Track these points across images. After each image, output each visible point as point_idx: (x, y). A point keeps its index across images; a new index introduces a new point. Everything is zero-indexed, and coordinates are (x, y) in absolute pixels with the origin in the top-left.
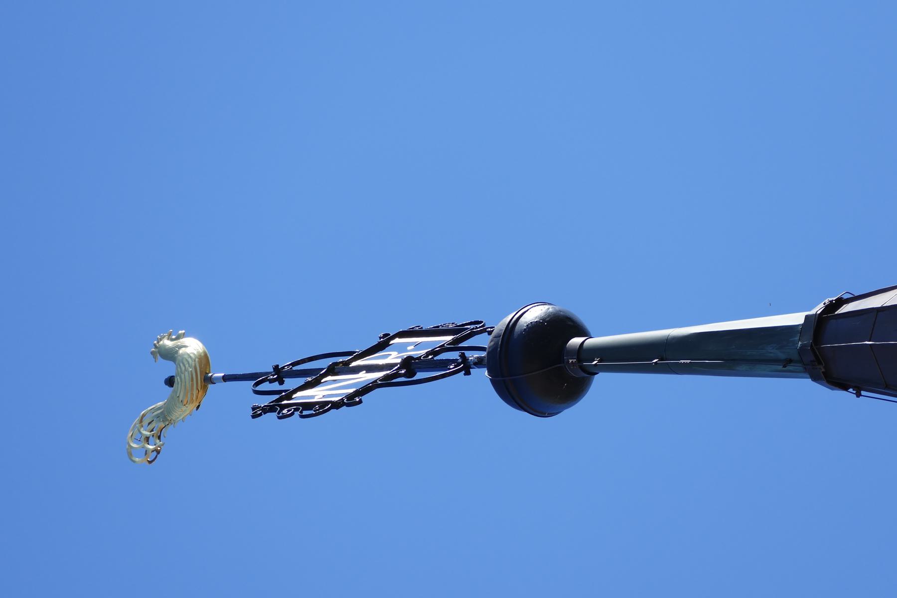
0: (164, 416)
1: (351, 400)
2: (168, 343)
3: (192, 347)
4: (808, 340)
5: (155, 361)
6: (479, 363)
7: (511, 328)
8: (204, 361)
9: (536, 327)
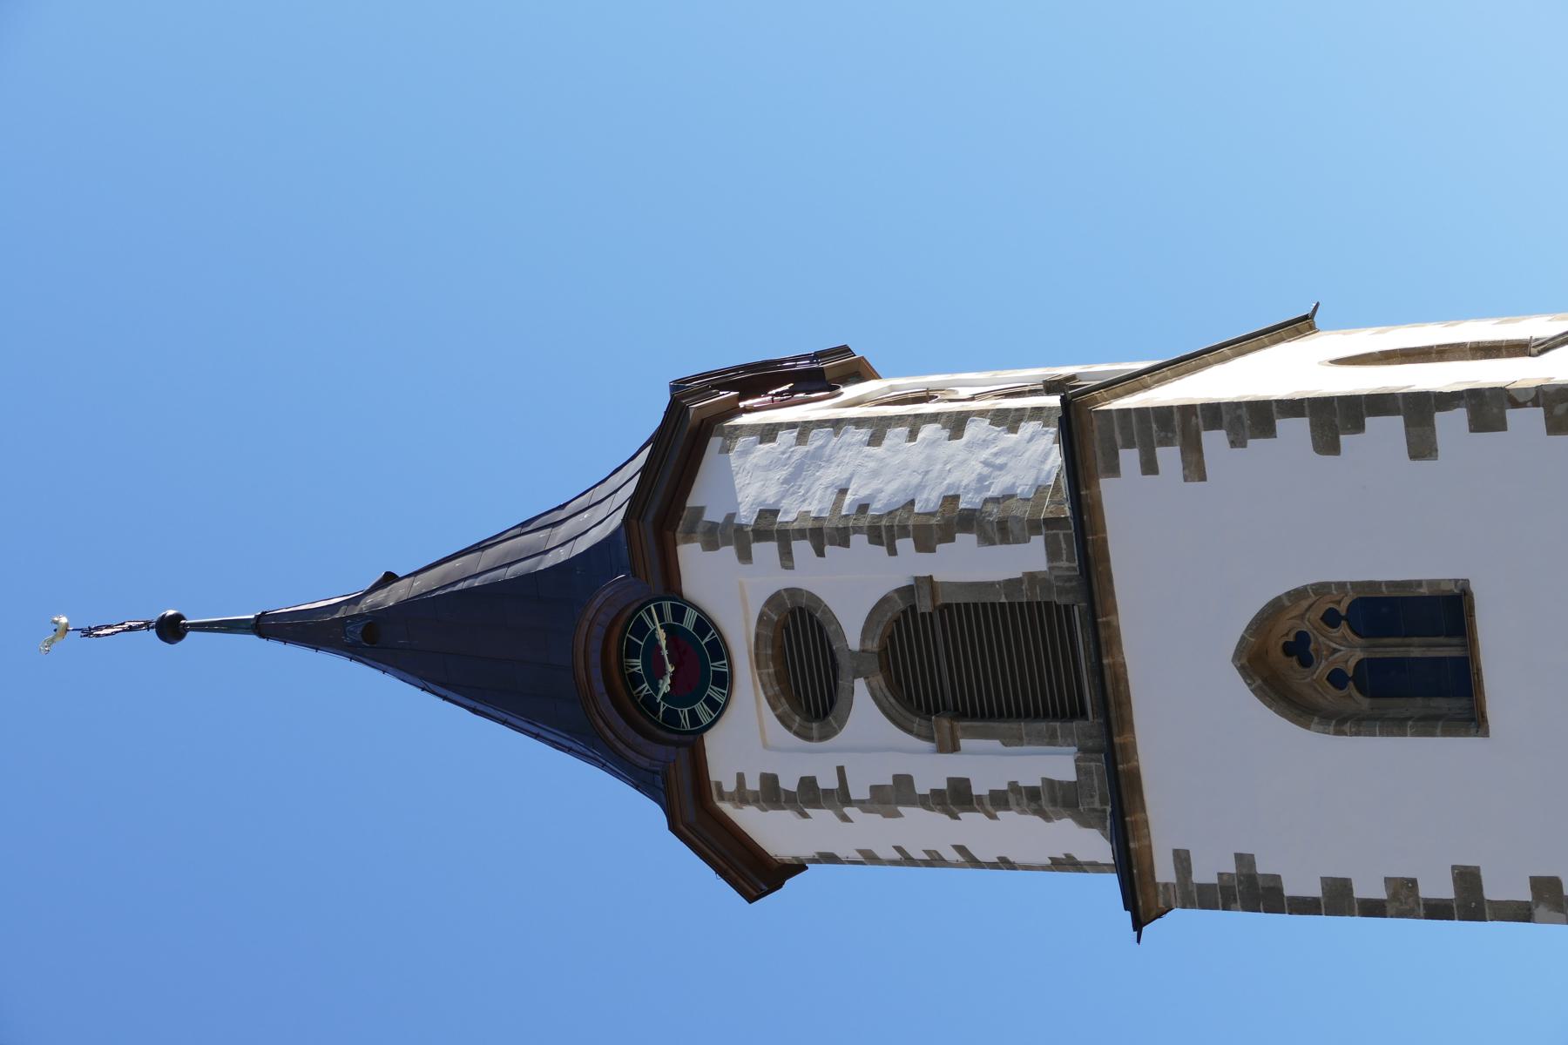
0: (53, 640)
1: (112, 634)
2: (56, 619)
3: (64, 620)
4: (255, 622)
5: (1139, 941)
6: (152, 628)
7: (164, 616)
8: (67, 625)
9: (171, 616)
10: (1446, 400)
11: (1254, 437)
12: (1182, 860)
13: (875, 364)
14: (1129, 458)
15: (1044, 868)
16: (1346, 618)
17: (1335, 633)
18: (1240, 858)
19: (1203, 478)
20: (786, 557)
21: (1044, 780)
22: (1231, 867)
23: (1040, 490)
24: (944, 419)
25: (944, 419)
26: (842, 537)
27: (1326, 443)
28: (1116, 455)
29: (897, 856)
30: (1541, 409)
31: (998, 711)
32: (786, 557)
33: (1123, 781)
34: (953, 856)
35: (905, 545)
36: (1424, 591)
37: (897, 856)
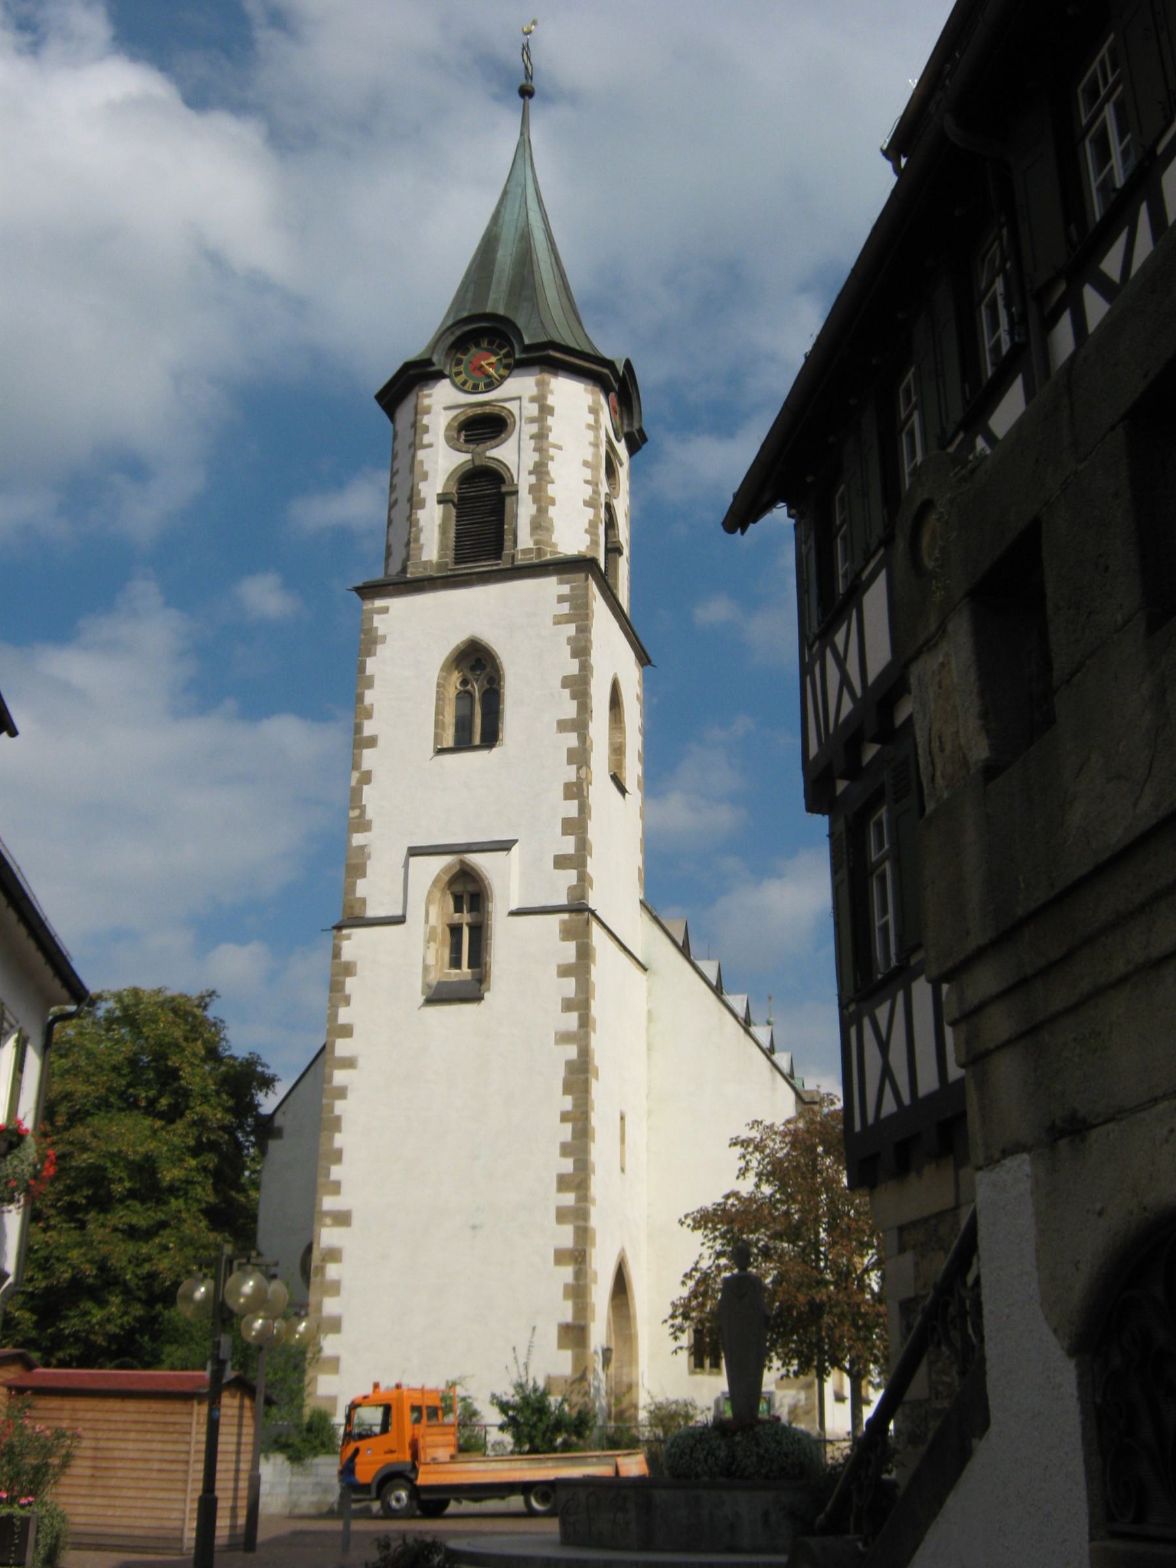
10: (583, 738)
11: (572, 648)
12: (385, 610)
13: (635, 457)
14: (565, 589)
15: (387, 541)
16: (491, 687)
17: (485, 683)
18: (384, 637)
19: (555, 624)
20: (532, 420)
21: (423, 545)
22: (380, 632)
23: (554, 545)
24: (595, 496)
25: (595, 496)
26: (539, 449)
27: (567, 682)
28: (567, 583)
29: (394, 470)
30: (575, 781)
31: (639, 435)
32: (532, 420)
33: (420, 584)
34: (394, 496)
35: (533, 479)
36: (500, 725)
37: (394, 470)
